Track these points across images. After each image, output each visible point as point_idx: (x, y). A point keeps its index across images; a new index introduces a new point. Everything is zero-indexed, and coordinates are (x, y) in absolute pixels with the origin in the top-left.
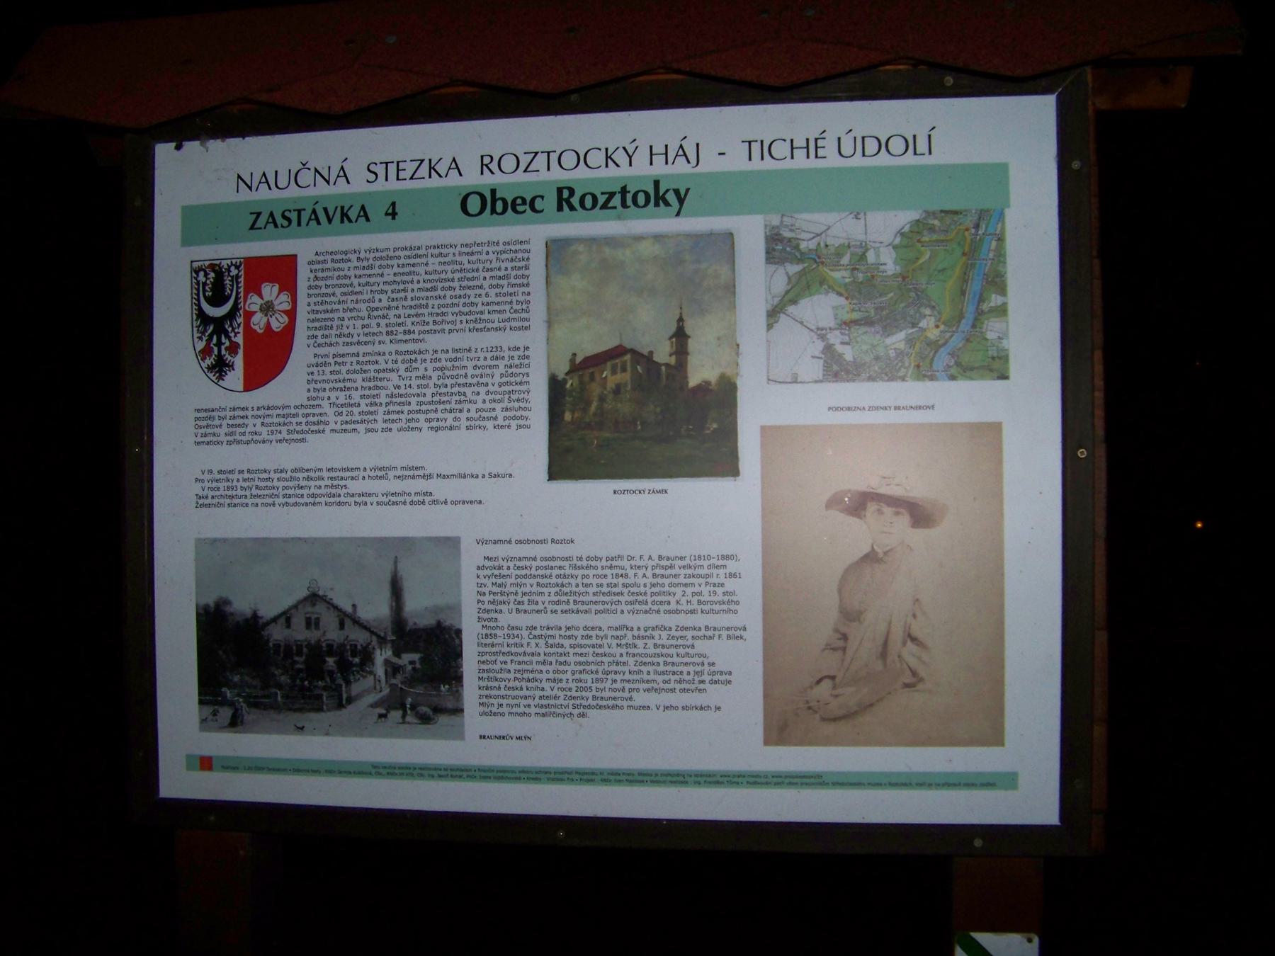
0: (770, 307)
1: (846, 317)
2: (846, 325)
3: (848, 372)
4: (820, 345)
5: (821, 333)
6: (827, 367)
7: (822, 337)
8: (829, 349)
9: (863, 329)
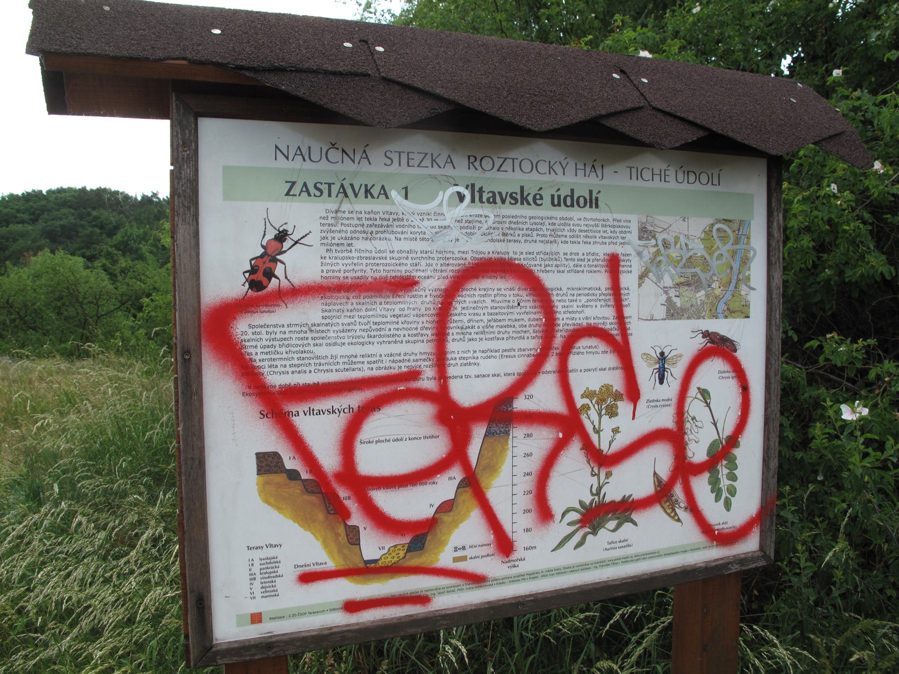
0: (640, 273)
1: (678, 280)
2: (678, 285)
3: (678, 313)
4: (665, 297)
5: (666, 290)
6: (668, 310)
7: (666, 293)
8: (669, 299)
9: (686, 288)
